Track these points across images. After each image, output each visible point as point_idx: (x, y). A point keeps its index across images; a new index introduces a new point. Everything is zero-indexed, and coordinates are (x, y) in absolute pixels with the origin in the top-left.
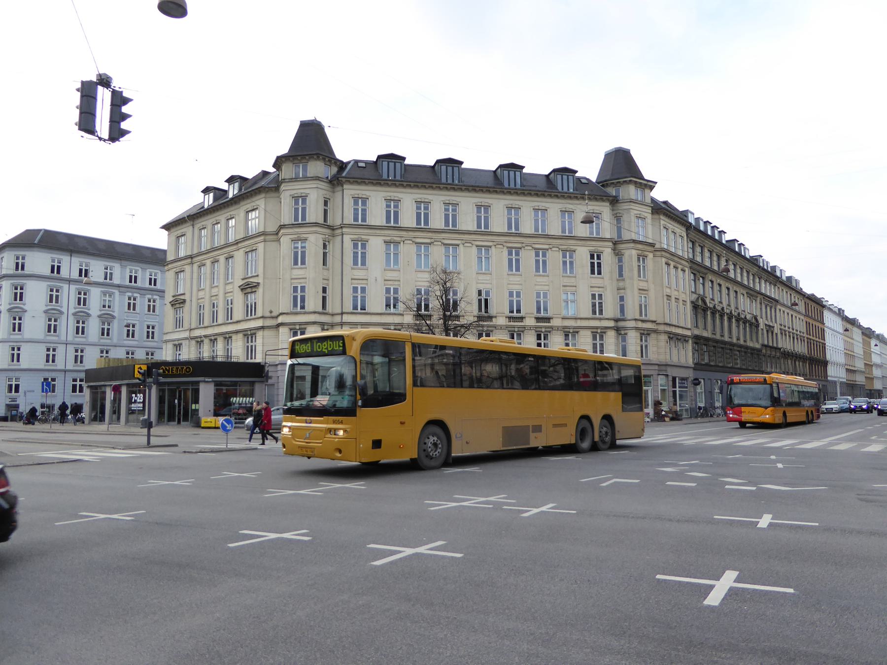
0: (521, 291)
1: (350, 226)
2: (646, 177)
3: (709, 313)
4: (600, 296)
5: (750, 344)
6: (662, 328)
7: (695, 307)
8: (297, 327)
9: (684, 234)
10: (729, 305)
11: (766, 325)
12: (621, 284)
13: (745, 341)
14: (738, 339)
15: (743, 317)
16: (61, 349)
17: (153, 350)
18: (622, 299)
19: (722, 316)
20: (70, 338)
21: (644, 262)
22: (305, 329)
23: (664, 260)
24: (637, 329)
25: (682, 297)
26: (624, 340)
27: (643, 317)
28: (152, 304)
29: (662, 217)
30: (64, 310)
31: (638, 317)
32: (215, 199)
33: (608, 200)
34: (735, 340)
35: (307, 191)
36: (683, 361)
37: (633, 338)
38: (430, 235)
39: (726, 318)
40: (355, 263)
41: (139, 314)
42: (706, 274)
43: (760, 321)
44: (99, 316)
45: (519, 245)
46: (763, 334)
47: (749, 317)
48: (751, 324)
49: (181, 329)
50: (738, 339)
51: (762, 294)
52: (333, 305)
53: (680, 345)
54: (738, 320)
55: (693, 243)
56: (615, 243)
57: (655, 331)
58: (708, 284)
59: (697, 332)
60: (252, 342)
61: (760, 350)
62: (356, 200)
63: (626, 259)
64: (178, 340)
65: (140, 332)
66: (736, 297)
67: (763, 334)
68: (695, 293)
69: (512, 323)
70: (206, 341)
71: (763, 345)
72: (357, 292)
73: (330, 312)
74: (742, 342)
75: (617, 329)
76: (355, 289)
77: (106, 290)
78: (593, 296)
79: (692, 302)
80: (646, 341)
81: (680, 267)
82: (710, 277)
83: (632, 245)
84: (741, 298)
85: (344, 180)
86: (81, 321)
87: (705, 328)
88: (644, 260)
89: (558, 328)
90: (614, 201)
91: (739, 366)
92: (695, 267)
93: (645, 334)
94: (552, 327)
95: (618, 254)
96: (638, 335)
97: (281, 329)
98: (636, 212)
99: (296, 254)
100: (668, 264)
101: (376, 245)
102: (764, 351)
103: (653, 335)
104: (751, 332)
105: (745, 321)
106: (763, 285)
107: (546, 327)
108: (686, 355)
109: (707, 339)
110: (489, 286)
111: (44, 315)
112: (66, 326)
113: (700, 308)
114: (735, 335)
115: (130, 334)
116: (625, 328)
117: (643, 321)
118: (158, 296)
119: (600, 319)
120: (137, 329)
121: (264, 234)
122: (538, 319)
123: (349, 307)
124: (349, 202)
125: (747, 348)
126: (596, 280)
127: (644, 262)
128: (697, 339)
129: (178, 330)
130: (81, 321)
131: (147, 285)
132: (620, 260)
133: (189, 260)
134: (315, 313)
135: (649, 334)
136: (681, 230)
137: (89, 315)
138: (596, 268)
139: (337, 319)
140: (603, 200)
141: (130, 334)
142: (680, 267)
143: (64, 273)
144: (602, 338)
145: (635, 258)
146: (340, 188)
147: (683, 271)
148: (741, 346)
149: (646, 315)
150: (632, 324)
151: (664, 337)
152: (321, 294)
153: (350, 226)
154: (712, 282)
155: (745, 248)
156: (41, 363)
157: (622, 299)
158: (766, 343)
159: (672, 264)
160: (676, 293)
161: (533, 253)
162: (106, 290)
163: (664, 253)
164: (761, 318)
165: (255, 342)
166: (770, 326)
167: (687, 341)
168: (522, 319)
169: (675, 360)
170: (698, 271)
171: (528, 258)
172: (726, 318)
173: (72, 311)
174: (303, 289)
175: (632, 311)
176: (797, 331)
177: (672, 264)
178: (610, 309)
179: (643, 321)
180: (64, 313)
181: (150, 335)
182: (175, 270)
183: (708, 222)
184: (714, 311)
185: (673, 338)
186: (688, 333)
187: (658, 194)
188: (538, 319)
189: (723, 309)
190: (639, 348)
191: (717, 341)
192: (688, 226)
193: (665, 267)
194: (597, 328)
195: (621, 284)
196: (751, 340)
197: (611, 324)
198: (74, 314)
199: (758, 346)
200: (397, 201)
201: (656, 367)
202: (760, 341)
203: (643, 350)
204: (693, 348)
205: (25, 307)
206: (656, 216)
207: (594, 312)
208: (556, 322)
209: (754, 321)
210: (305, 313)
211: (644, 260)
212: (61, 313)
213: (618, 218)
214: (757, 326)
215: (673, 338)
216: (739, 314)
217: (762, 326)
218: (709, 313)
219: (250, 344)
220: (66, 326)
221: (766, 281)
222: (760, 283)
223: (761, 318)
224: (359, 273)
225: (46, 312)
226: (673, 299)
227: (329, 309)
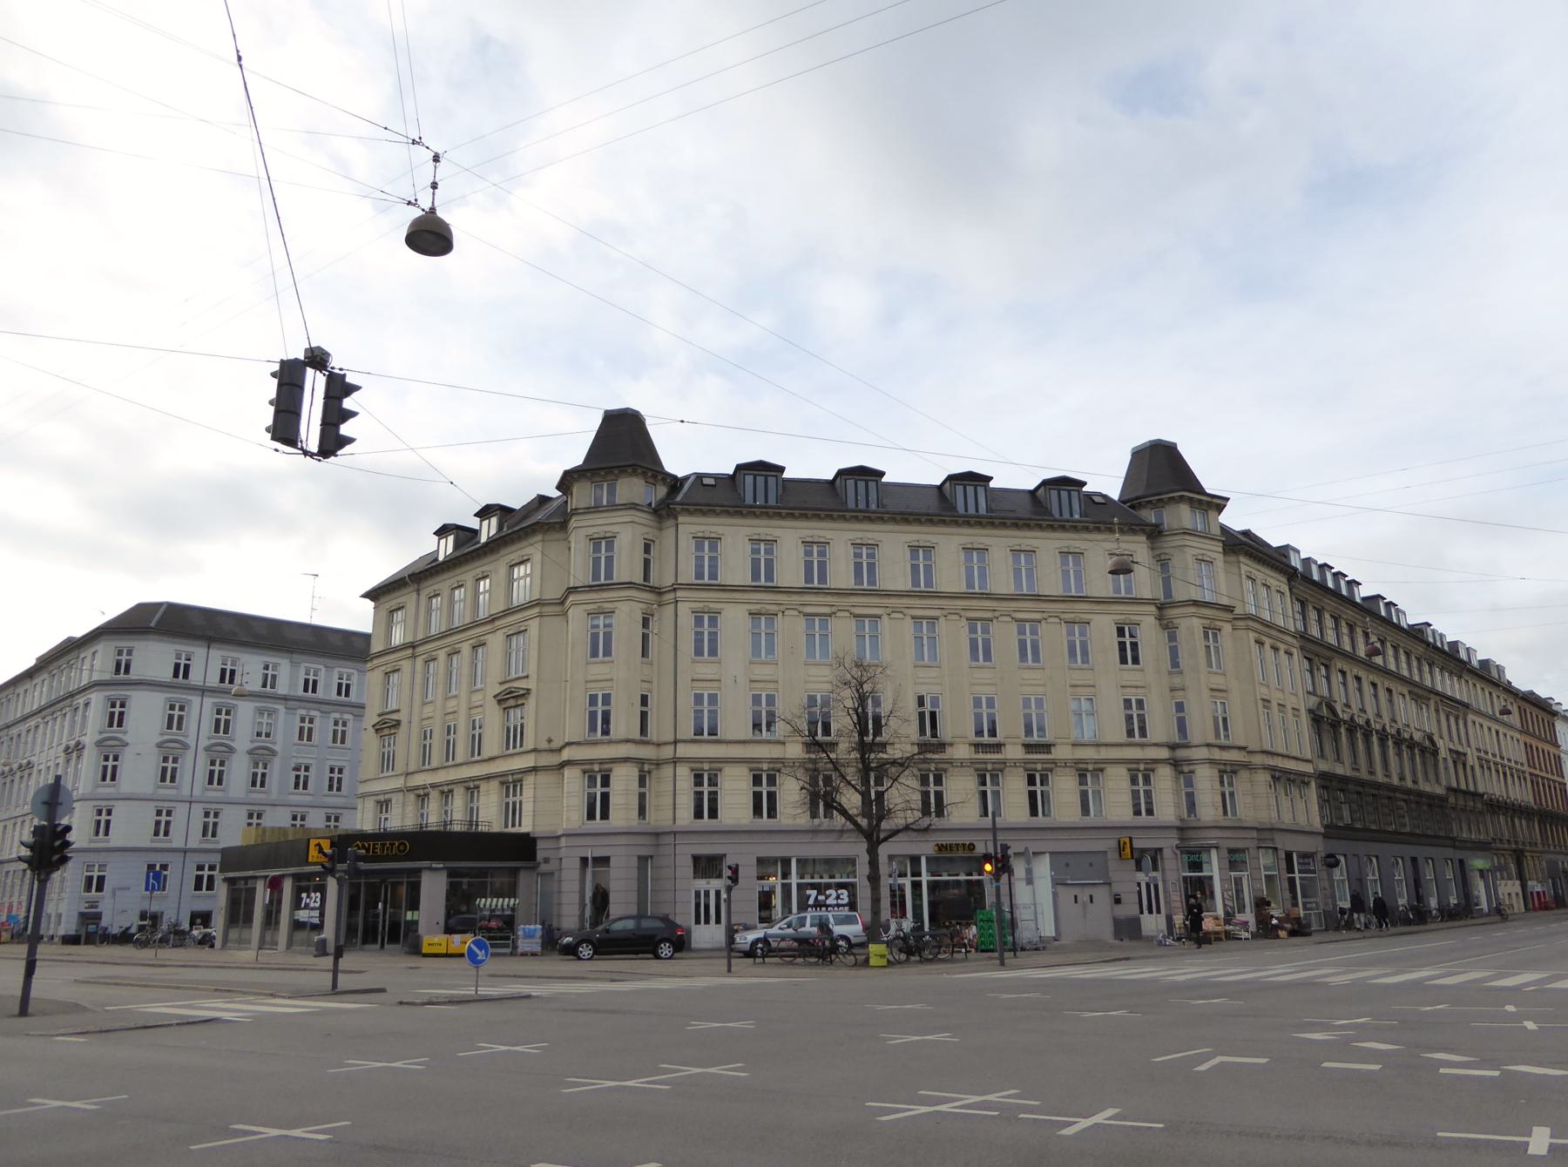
0: (649, 695)
1: (689, 587)
2: (1208, 491)
3: (1343, 730)
4: (1140, 703)
5: (1426, 787)
6: (1258, 760)
7: (1316, 719)
8: (596, 768)
9: (1285, 588)
10: (1379, 715)
11: (1450, 750)
12: (1177, 681)
13: (1415, 782)
14: (1402, 778)
15: (1407, 736)
16: (180, 812)
17: (339, 811)
18: (1180, 707)
19: (1367, 737)
20: (197, 792)
21: (1216, 641)
22: (611, 770)
23: (1252, 636)
24: (1212, 762)
25: (1291, 702)
26: (1189, 783)
27: (1223, 741)
28: (307, 725)
29: (1242, 559)
30: (191, 741)
31: (1212, 740)
32: (457, 546)
33: (1144, 531)
34: (1395, 781)
35: (615, 529)
36: (1302, 821)
37: (1205, 779)
38: (830, 599)
39: (1375, 739)
40: (699, 651)
41: (317, 746)
42: (1330, 659)
43: (1440, 743)
44: (250, 752)
45: (989, 615)
46: (1446, 768)
47: (1417, 736)
48: (1423, 750)
49: (391, 773)
50: (1402, 778)
51: (1437, 694)
52: (660, 728)
53: (1295, 792)
54: (1399, 742)
55: (1303, 604)
56: (1161, 607)
57: (1247, 766)
58: (1337, 678)
59: (1324, 766)
60: (514, 795)
61: (1443, 800)
62: (699, 541)
63: (1182, 633)
64: (385, 794)
65: (319, 778)
66: (1391, 701)
67: (1446, 768)
68: (1314, 693)
69: (981, 756)
70: (434, 794)
71: (1449, 789)
72: (702, 703)
73: (655, 739)
74: (1409, 784)
75: (1176, 764)
76: (698, 699)
77: (223, 700)
78: (1127, 703)
79: (1310, 711)
80: (1231, 784)
81: (1282, 647)
82: (1340, 664)
83: (1192, 610)
84: (1399, 702)
85: (678, 508)
86: (219, 758)
87: (1338, 759)
88: (1215, 635)
89: (1066, 764)
90: (1155, 533)
91: (1408, 829)
92: (1310, 646)
93: (1228, 771)
94: (1054, 762)
95: (1168, 626)
96: (1216, 773)
97: (567, 771)
98: (1196, 552)
99: (595, 637)
100: (1259, 643)
101: (734, 618)
102: (1452, 800)
103: (1244, 774)
104: (1424, 763)
105: (1412, 744)
106: (1438, 678)
107: (1043, 762)
108: (1306, 811)
109: (1344, 780)
110: (936, 689)
111: (156, 750)
112: (193, 770)
113: (1325, 721)
114: (1396, 770)
115: (301, 783)
116: (1189, 761)
117: (1222, 748)
118: (319, 710)
119: (1142, 745)
120: (312, 773)
121: (538, 603)
122: (1029, 747)
123: (687, 730)
124: (687, 545)
125: (1420, 794)
126: (1130, 674)
127: (1216, 641)
128: (1327, 782)
129: (385, 774)
130: (219, 758)
131: (333, 696)
132: (1172, 638)
133: (410, 651)
134: (628, 741)
135: (1234, 772)
136: (1278, 582)
137: (231, 750)
138: (1129, 653)
139: (667, 752)
140: (1134, 532)
141: (301, 783)
142: (1282, 647)
143: (196, 677)
144: (1147, 780)
145: (1199, 633)
146: (671, 522)
147: (1289, 654)
148: (1408, 792)
149: (1227, 736)
150: (1202, 753)
151: (1263, 778)
152: (638, 708)
153: (689, 587)
154: (1343, 673)
155: (1398, 611)
156: (144, 838)
157: (1180, 707)
158: (1454, 785)
159: (1268, 642)
160: (1280, 695)
161: (1014, 627)
162: (223, 700)
163: (1251, 623)
164: (1441, 737)
165: (521, 795)
166: (1457, 753)
167: (1308, 784)
168: (998, 747)
169: (1287, 820)
170: (1317, 654)
171: (1004, 636)
172: (1375, 739)
173: (204, 743)
174: (607, 699)
175: (1200, 729)
176: (1509, 760)
177: (1268, 642)
178: (1160, 727)
179: (1222, 748)
180: (190, 747)
181: (335, 785)
182: (383, 668)
183: (1325, 565)
184: (1352, 727)
185: (1281, 778)
186: (1309, 768)
187: (1232, 519)
188: (1029, 747)
189: (1368, 722)
190: (1219, 799)
191: (1361, 783)
192: (1291, 574)
193: (1255, 648)
194: (1138, 761)
195: (1177, 681)
196: (1427, 779)
197: (1164, 753)
198: (207, 749)
199: (1440, 791)
200: (771, 542)
201: (1254, 834)
202: (1444, 783)
203: (1226, 801)
204: (1320, 797)
205: (126, 738)
206: (1232, 558)
207: (1130, 733)
208: (1060, 753)
209: (1427, 743)
210: (610, 742)
211: (1215, 635)
212: (185, 747)
213: (1163, 563)
214: (1435, 753)
215: (1281, 778)
216: (1398, 731)
217: (1443, 753)
218: (1343, 730)
219: (511, 799)
220: (193, 770)
221: (1442, 669)
222: (1431, 673)
223: (1441, 737)
224: (706, 670)
225: (159, 745)
226: (1274, 705)
227: (653, 734)
